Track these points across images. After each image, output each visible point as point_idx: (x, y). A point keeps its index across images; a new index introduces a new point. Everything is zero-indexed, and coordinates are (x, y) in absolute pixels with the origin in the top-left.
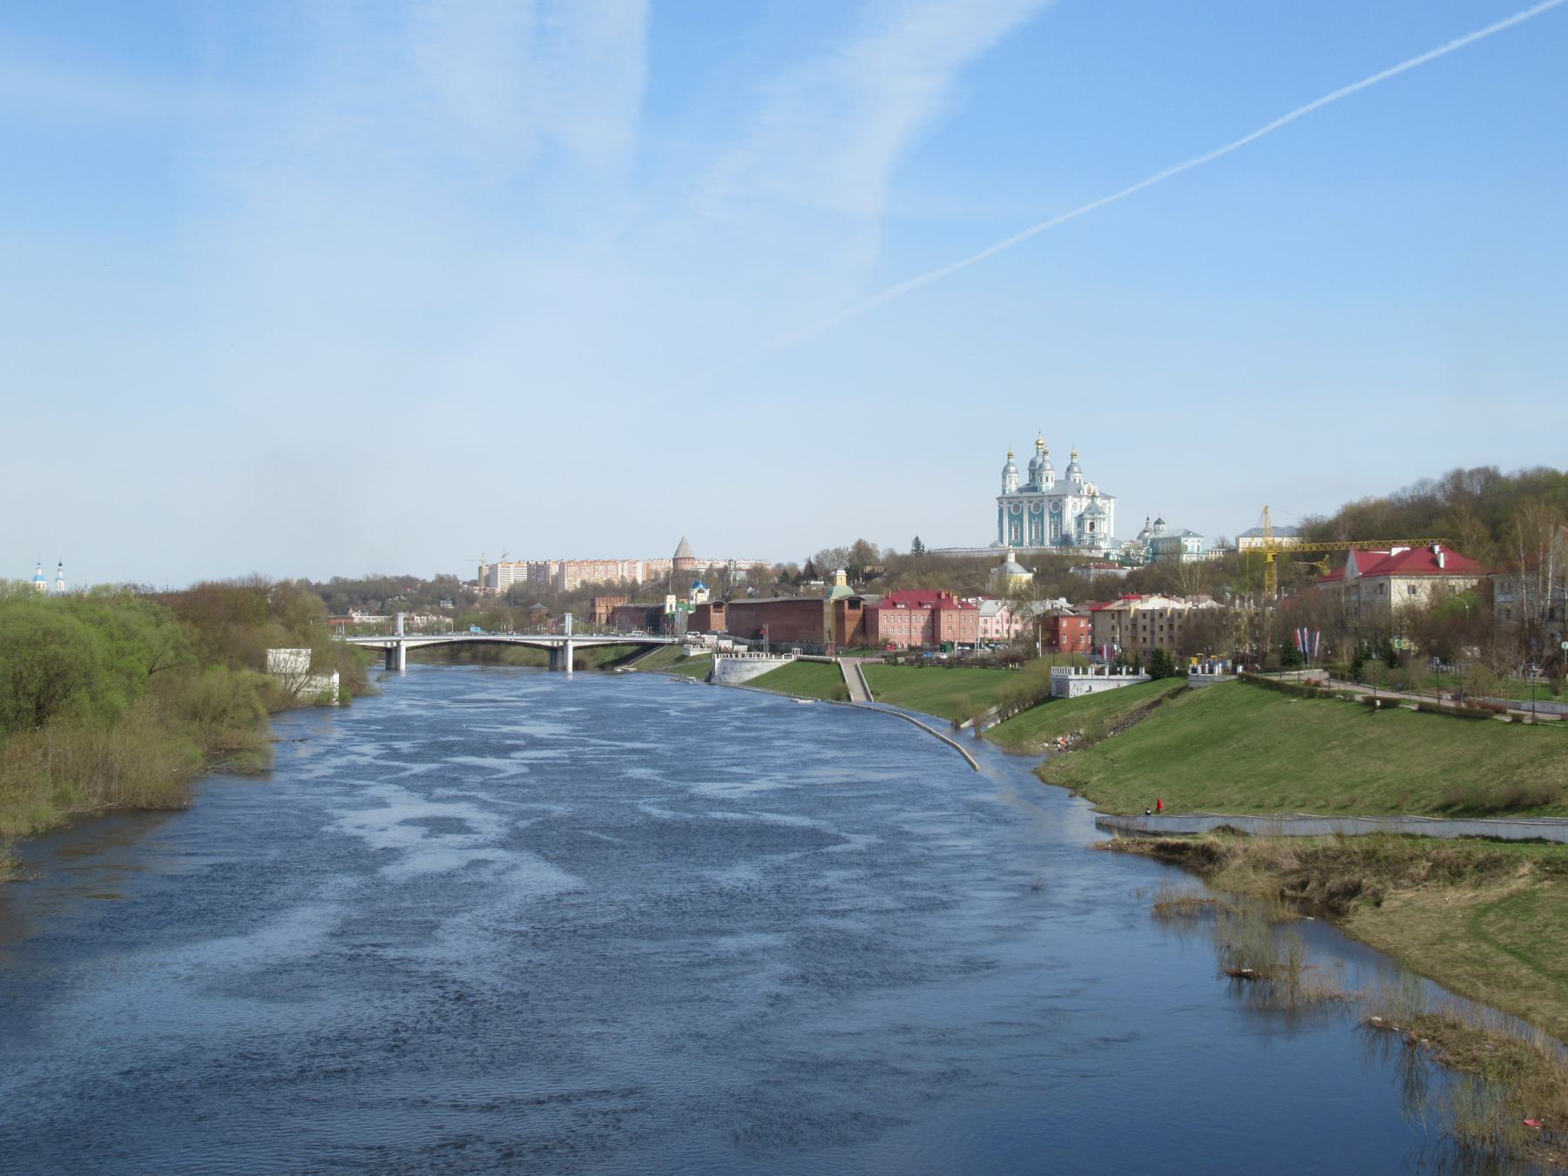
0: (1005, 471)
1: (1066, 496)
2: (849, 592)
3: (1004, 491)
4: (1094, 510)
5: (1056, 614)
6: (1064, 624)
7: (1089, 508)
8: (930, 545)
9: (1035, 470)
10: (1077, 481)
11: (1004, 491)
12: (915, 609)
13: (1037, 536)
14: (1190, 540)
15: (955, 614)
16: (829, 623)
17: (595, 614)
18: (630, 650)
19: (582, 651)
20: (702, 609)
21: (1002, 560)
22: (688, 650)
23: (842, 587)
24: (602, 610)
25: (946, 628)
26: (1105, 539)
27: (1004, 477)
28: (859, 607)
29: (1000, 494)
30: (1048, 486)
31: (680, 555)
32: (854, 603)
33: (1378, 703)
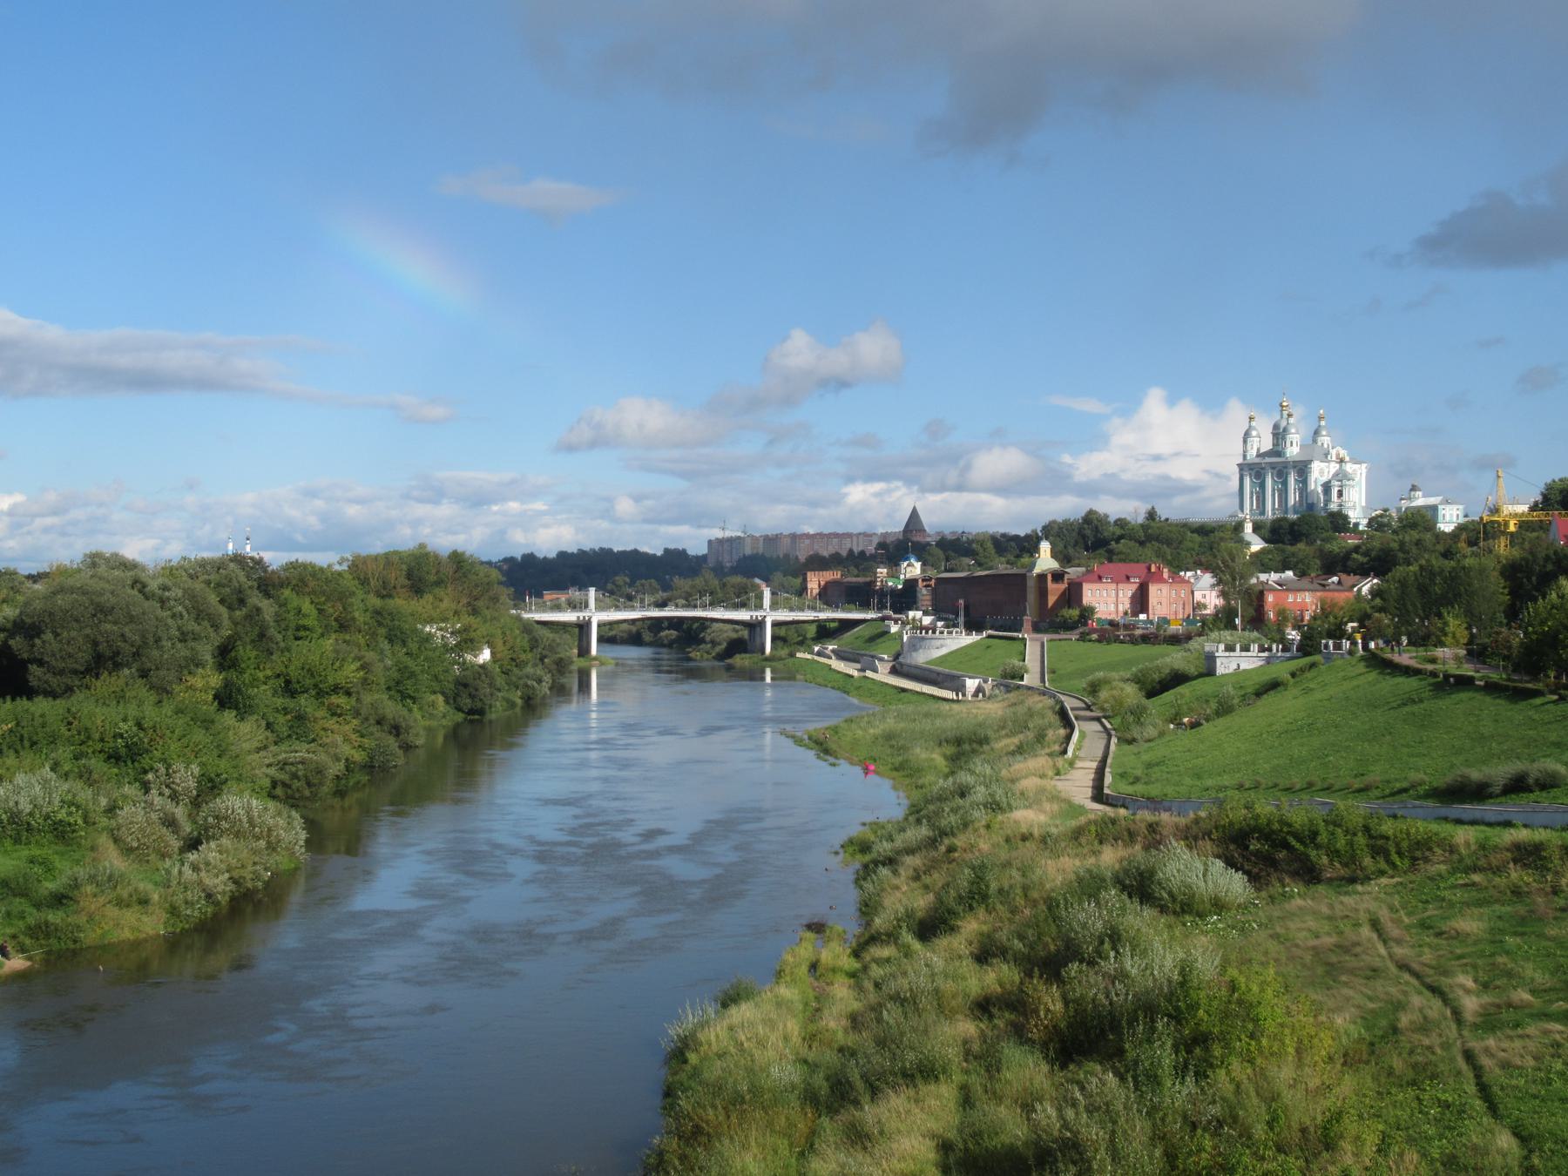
0: (1247, 435)
1: (1310, 461)
2: (1054, 565)
3: (1245, 457)
4: (1341, 476)
5: (1261, 588)
6: (1270, 598)
7: (1336, 475)
8: (1163, 513)
9: (1278, 434)
10: (1326, 446)
11: (1245, 457)
12: (1122, 582)
13: (1258, 506)
14: (1448, 507)
15: (1165, 588)
16: (1032, 596)
17: (806, 588)
18: (833, 625)
19: (1052, 643)
20: (911, 584)
21: (1239, 527)
22: (889, 626)
23: (1045, 560)
24: (814, 582)
25: (1155, 604)
26: (1354, 507)
27: (1245, 442)
28: (1063, 580)
29: (1240, 460)
30: (1293, 451)
31: (911, 528)
32: (1058, 576)
33: (1452, 680)
